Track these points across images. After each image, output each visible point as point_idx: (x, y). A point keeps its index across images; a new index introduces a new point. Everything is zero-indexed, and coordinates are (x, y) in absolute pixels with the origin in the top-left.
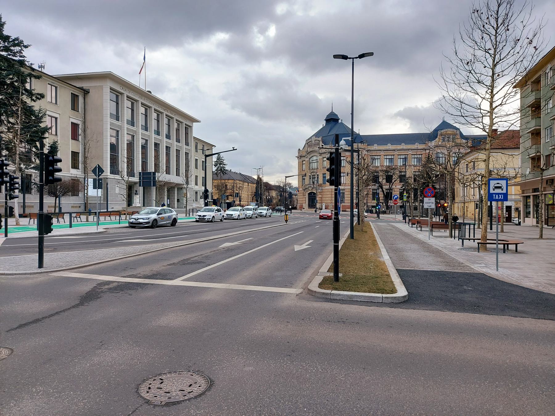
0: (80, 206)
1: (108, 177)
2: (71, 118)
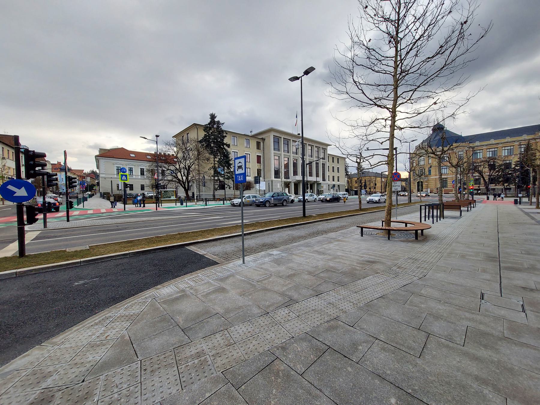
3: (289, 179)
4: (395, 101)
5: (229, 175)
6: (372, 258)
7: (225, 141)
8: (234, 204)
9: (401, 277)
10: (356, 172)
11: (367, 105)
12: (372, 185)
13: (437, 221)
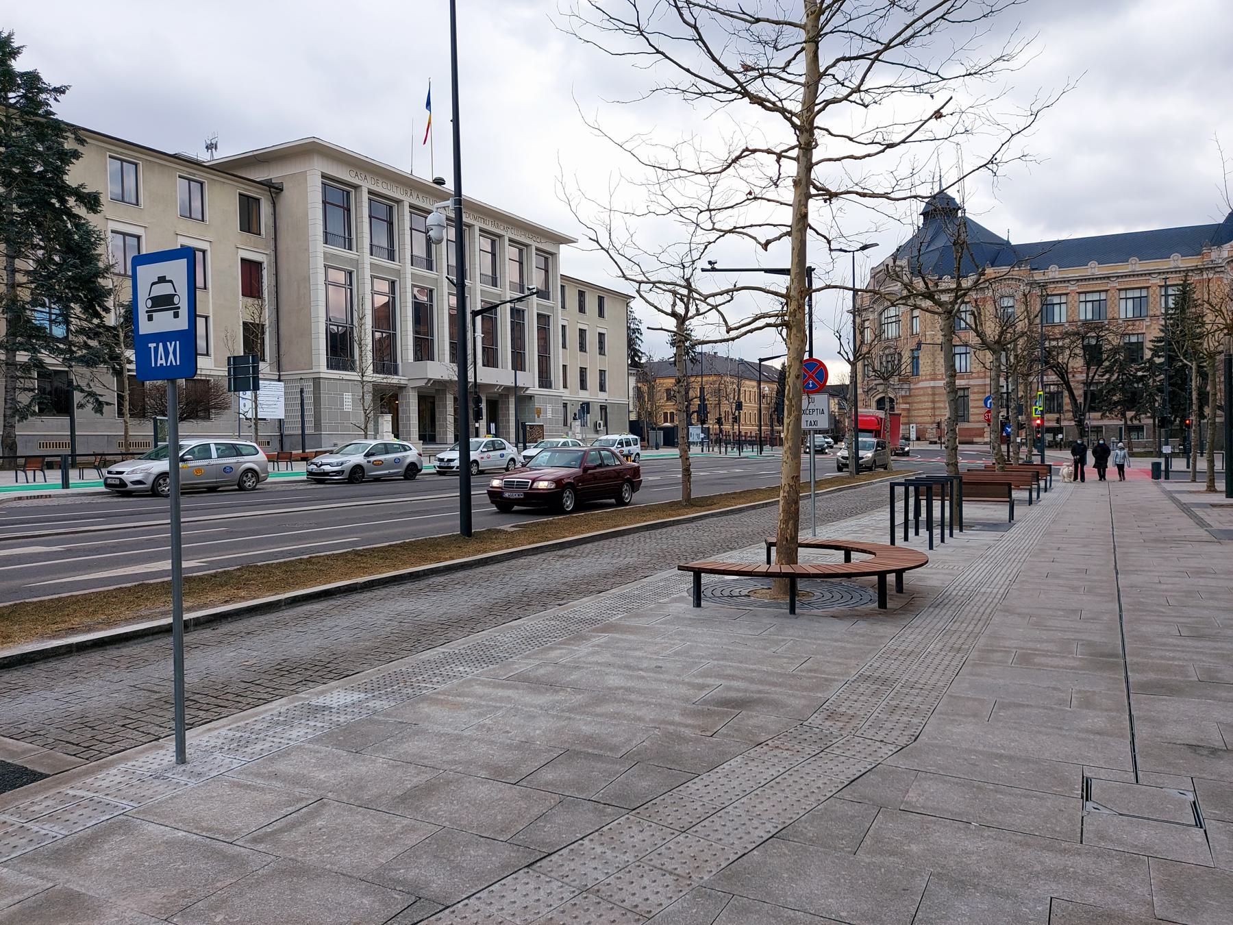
0: (268, 442)
1: (322, 375)
2: (239, 250)
3: (396, 373)
4: (812, 87)
5: (93, 343)
6: (738, 688)
7: (74, 175)
8: (123, 484)
9: (838, 752)
10: (669, 353)
11: (712, 89)
12: (726, 407)
13: (943, 541)
